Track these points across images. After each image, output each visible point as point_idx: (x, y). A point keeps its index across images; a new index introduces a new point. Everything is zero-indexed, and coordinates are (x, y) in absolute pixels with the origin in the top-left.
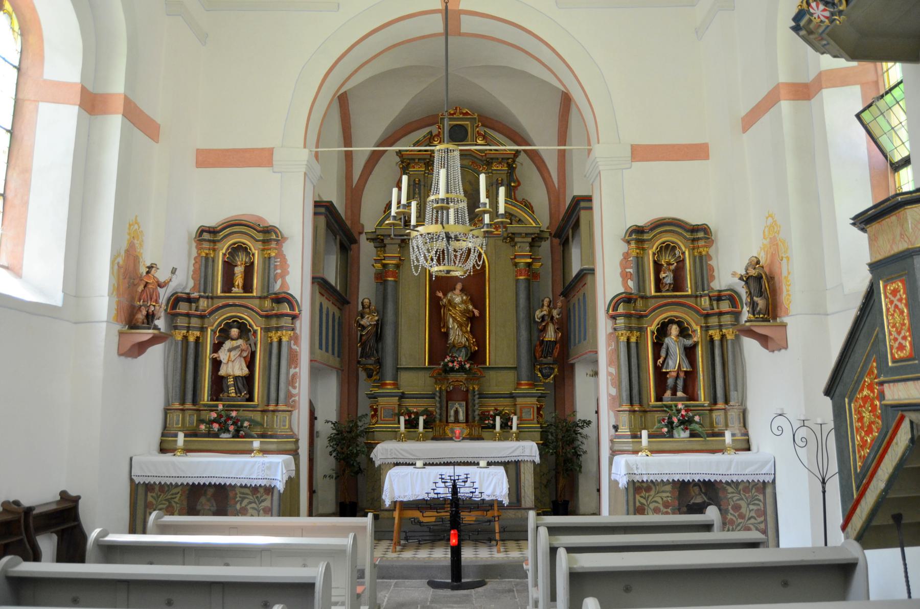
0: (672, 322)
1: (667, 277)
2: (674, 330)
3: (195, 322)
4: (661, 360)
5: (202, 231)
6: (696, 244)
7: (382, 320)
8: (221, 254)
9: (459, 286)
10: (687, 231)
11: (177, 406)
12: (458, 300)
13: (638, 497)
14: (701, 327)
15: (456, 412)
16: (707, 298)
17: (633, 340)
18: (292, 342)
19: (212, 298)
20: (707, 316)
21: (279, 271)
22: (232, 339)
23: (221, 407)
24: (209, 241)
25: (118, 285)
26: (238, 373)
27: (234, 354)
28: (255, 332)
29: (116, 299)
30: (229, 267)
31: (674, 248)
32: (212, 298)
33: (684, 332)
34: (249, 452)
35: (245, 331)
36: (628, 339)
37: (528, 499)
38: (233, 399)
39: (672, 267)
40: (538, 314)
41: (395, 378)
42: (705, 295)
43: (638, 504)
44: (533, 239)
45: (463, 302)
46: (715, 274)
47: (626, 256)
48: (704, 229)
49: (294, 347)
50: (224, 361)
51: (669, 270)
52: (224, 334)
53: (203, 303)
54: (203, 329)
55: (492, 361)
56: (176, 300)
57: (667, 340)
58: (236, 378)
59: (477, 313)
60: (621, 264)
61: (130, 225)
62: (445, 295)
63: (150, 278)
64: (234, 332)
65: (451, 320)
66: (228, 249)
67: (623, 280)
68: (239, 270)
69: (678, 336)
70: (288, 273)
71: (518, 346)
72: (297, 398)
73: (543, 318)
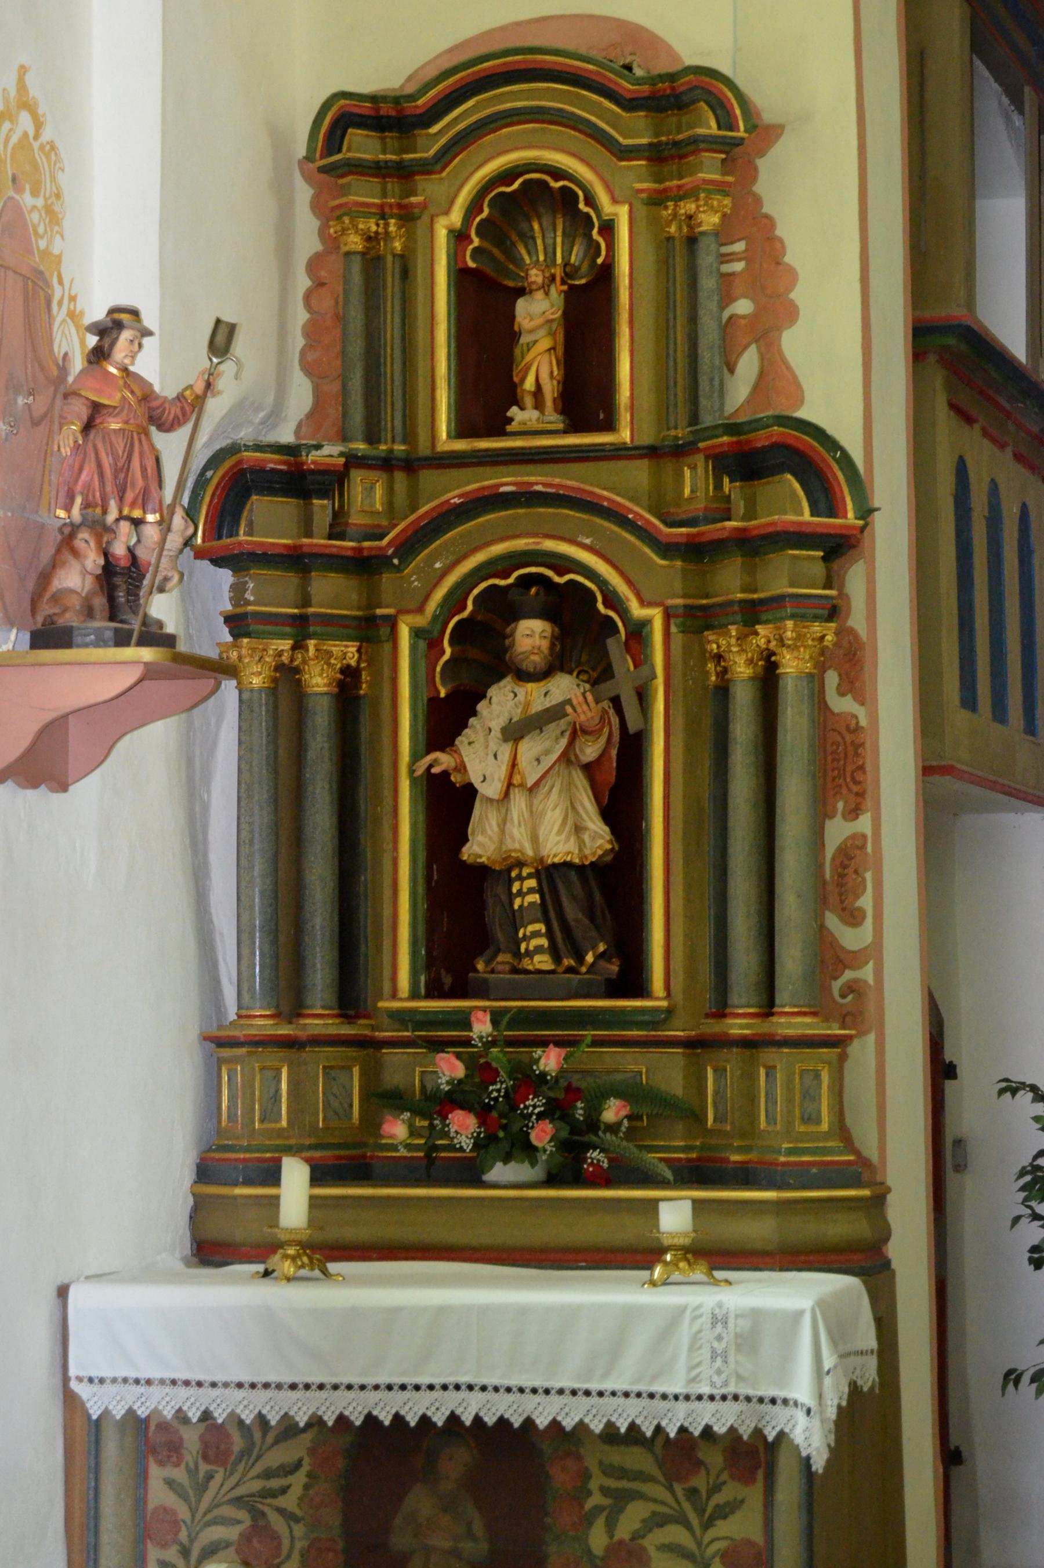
5: (346, 119)
18: (832, 679)
19: (411, 465)
21: (743, 307)
22: (523, 676)
23: (482, 1027)
26: (558, 846)
27: (537, 752)
28: (638, 633)
30: (486, 300)
32: (411, 465)
35: (585, 629)
49: (841, 704)
50: (490, 789)
52: (478, 654)
53: (368, 496)
54: (371, 629)
58: (550, 874)
64: (532, 635)
66: (474, 207)
68: (537, 313)
72: (867, 974)
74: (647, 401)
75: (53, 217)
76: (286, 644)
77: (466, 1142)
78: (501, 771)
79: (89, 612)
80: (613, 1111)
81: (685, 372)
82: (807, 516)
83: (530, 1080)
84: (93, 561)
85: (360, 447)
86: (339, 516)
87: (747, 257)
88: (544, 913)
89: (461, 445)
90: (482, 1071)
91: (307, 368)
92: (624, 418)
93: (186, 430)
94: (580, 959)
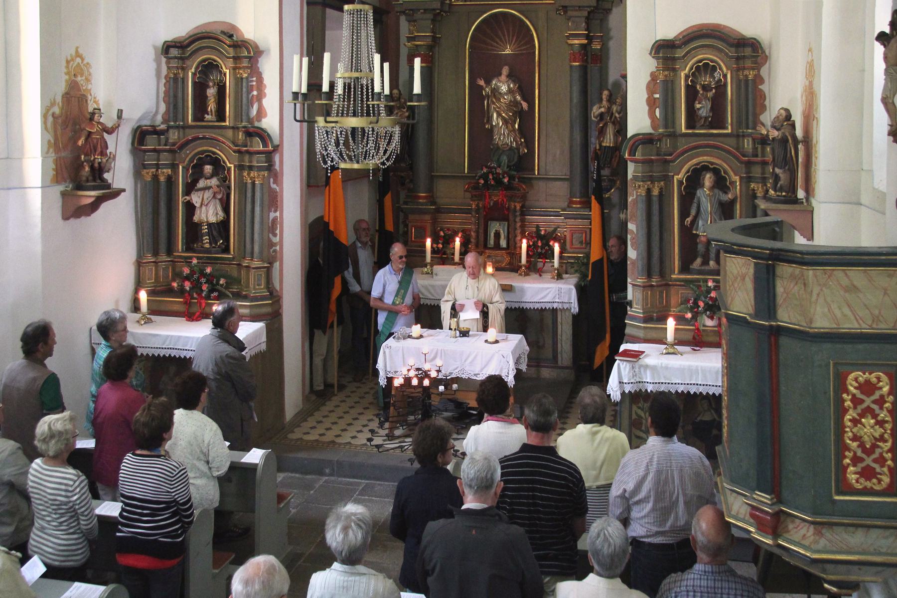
0: (705, 168)
1: (703, 108)
2: (708, 179)
3: (165, 159)
4: (689, 220)
5: (167, 47)
8: (190, 74)
9: (505, 71)
10: (732, 45)
12: (504, 88)
13: (634, 408)
14: (741, 178)
15: (497, 235)
16: (750, 140)
18: (272, 180)
19: (184, 127)
20: (749, 164)
21: (255, 93)
22: (206, 179)
23: (195, 261)
24: (176, 58)
25: (56, 139)
26: (213, 219)
27: (208, 194)
28: (229, 169)
29: (52, 155)
31: (714, 69)
33: (721, 183)
35: (217, 164)
36: (649, 191)
37: (565, 356)
38: (208, 251)
39: (710, 94)
40: (596, 110)
41: (430, 190)
42: (749, 135)
43: (634, 416)
44: (589, 13)
45: (510, 91)
46: (767, 103)
49: (274, 186)
50: (197, 205)
51: (706, 98)
52: (197, 173)
53: (173, 136)
54: (174, 167)
55: (543, 171)
56: (141, 135)
57: (699, 193)
58: (210, 225)
59: (525, 105)
61: (68, 62)
62: (488, 82)
63: (92, 126)
64: (208, 169)
65: (495, 115)
66: (197, 68)
68: (211, 92)
69: (712, 188)
70: (265, 95)
72: (278, 248)
73: (601, 115)
74: (232, 117)
75: (88, 80)
76: (154, 170)
77: (188, 289)
78: (200, 201)
79: (87, 181)
80: (222, 281)
82: (261, 148)
83: (203, 274)
84: (87, 169)
86: (167, 139)
87: (257, 81)
89: (194, 124)
90: (193, 272)
91: (164, 101)
92: (227, 119)
93: (114, 135)
94: (216, 244)
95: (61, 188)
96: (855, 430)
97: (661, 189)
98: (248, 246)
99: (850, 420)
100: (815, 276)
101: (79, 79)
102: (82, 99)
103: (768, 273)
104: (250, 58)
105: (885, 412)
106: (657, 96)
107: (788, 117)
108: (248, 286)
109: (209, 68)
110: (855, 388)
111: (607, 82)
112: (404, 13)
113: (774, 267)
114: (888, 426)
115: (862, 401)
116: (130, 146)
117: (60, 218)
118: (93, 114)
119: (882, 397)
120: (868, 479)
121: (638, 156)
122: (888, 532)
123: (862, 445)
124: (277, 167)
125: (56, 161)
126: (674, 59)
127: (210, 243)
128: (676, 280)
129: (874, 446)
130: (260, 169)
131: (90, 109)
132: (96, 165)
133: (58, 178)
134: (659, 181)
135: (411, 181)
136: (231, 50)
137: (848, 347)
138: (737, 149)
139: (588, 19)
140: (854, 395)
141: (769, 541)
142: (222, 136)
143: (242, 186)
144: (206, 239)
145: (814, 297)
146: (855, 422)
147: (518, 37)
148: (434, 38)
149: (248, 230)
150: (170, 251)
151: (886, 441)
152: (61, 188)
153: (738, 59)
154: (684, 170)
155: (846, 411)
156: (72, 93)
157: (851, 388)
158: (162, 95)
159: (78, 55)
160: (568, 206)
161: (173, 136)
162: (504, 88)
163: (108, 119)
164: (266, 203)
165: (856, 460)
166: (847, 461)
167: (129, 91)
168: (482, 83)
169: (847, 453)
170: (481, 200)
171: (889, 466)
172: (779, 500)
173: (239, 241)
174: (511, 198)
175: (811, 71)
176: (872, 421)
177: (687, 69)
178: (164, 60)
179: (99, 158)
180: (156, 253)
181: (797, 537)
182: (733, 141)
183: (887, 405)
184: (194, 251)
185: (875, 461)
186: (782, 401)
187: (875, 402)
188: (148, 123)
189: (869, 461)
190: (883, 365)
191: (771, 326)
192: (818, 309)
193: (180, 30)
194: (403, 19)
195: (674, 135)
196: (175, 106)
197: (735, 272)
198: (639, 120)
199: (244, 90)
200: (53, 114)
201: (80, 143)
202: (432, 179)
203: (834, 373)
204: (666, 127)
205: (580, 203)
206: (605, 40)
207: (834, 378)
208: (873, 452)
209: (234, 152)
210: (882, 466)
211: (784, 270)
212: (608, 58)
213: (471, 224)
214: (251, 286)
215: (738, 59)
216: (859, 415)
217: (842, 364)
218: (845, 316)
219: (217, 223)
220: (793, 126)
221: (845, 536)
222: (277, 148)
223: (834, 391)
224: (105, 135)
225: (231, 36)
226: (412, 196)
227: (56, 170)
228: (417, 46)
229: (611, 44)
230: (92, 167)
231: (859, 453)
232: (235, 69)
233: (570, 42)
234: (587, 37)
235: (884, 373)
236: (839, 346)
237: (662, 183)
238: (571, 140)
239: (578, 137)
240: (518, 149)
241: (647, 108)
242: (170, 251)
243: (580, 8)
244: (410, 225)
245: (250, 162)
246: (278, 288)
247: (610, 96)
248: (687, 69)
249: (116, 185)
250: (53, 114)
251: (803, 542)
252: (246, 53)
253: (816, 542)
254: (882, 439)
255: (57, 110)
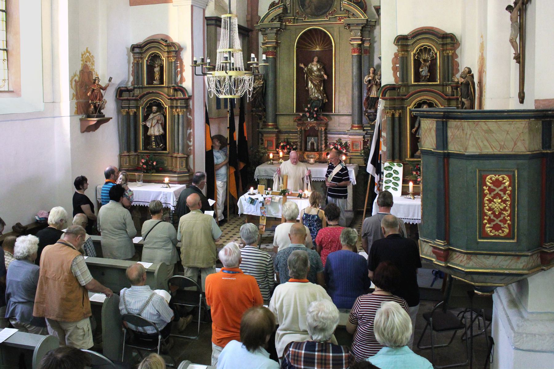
1: (424, 71)
3: (133, 104)
4: (414, 130)
5: (133, 48)
6: (445, 48)
7: (266, 84)
9: (316, 59)
10: (439, 38)
11: (126, 153)
12: (315, 68)
17: (397, 115)
19: (142, 88)
20: (449, 100)
21: (179, 69)
22: (154, 113)
24: (138, 53)
25: (77, 93)
26: (157, 134)
28: (166, 108)
29: (75, 101)
30: (151, 68)
31: (430, 50)
32: (142, 88)
34: (162, 182)
35: (160, 107)
36: (393, 115)
38: (154, 150)
39: (428, 64)
40: (366, 78)
41: (275, 121)
44: (362, 27)
45: (319, 70)
47: (396, 55)
48: (452, 37)
49: (190, 117)
50: (149, 127)
51: (426, 66)
52: (149, 111)
53: (137, 92)
54: (137, 108)
56: (120, 92)
58: (156, 137)
60: (393, 61)
61: (82, 55)
62: (306, 65)
64: (154, 108)
67: (394, 73)
68: (157, 70)
71: (353, 101)
73: (369, 81)
75: (93, 64)
79: (93, 113)
81: (170, 81)
84: (92, 107)
85: (136, 86)
88: (155, 141)
94: (159, 146)
95: (80, 117)
96: (490, 205)
97: (400, 114)
98: (176, 147)
99: (487, 200)
100: (469, 125)
101: (88, 63)
102: (90, 73)
103: (443, 126)
104: (176, 52)
105: (507, 195)
106: (398, 65)
107: (470, 71)
108: (176, 167)
109: (155, 57)
110: (490, 183)
111: (373, 65)
112: (261, 30)
113: (446, 122)
114: (509, 203)
115: (494, 190)
116: (115, 97)
117: (79, 132)
118: (95, 80)
119: (505, 188)
120: (497, 230)
121: (387, 96)
122: (507, 258)
123: (494, 213)
124: (191, 107)
125: (77, 104)
126: (407, 46)
127: (156, 146)
128: (408, 161)
129: (500, 213)
130: (181, 107)
131: (94, 78)
132: (97, 105)
133: (78, 112)
134: (399, 110)
135: (265, 117)
136: (166, 48)
137: (487, 162)
138: (443, 92)
139: (362, 31)
140: (489, 187)
141: (443, 265)
142: (162, 91)
143: (173, 117)
144: (154, 144)
145: (468, 136)
146: (490, 201)
147: (323, 42)
148: (277, 43)
149: (176, 139)
150: (136, 150)
151: (507, 211)
152: (80, 117)
153: (443, 45)
154: (413, 104)
155: (485, 195)
156: (85, 70)
157: (488, 183)
158: (131, 72)
159: (87, 51)
160: (351, 129)
161: (137, 92)
162: (315, 68)
163: (103, 82)
164: (185, 125)
165: (490, 221)
166: (486, 221)
167: (114, 69)
168: (302, 66)
169: (485, 217)
170: (303, 126)
171: (508, 224)
172: (449, 244)
173: (172, 146)
174: (319, 125)
175: (482, 47)
176: (500, 201)
177: (415, 51)
178: (132, 54)
179: (98, 103)
180: (129, 150)
181: (457, 262)
182: (440, 88)
183: (508, 192)
184: (148, 150)
185: (500, 221)
186: (451, 192)
187: (501, 190)
188: (124, 86)
189: (497, 221)
190: (506, 171)
191: (444, 153)
192: (470, 142)
193: (139, 39)
194: (260, 33)
195: (407, 86)
196: (138, 77)
197: (426, 127)
198: (388, 77)
199: (173, 68)
200: (75, 81)
201: (89, 94)
202: (276, 116)
203: (479, 176)
204: (403, 81)
205: (357, 127)
206: (372, 42)
207: (479, 179)
208: (500, 217)
209: (168, 99)
210: (505, 224)
211: (452, 123)
212: (373, 52)
213: (297, 139)
214: (178, 167)
215: (443, 45)
216: (492, 197)
217: (484, 171)
218: (485, 146)
219: (160, 136)
220: (472, 76)
221: (484, 260)
222: (190, 97)
223: (479, 185)
224: (102, 91)
225: (166, 41)
226: (265, 125)
227: (77, 108)
228: (267, 47)
229: (376, 45)
230: (95, 106)
231: (492, 217)
232: (168, 57)
233: (352, 43)
234: (362, 40)
235: (507, 176)
236: (481, 161)
237: (401, 111)
238: (353, 94)
239: (356, 93)
240: (323, 100)
241: (392, 72)
242: (136, 150)
243: (358, 25)
244: (264, 140)
245: (177, 104)
246: (192, 168)
247: (375, 70)
248: (415, 51)
249: (107, 116)
250: (75, 81)
251: (461, 264)
252: (175, 50)
253: (468, 263)
254: (504, 209)
255: (77, 78)
